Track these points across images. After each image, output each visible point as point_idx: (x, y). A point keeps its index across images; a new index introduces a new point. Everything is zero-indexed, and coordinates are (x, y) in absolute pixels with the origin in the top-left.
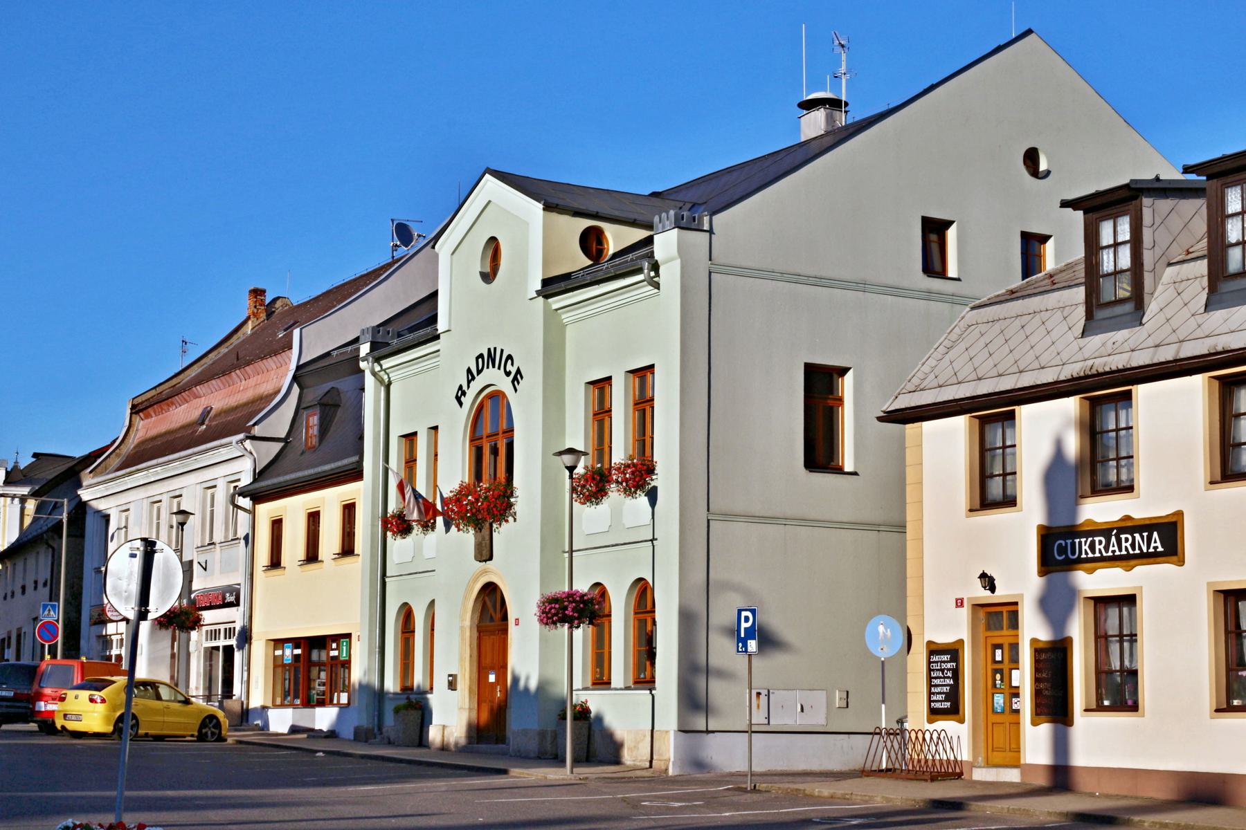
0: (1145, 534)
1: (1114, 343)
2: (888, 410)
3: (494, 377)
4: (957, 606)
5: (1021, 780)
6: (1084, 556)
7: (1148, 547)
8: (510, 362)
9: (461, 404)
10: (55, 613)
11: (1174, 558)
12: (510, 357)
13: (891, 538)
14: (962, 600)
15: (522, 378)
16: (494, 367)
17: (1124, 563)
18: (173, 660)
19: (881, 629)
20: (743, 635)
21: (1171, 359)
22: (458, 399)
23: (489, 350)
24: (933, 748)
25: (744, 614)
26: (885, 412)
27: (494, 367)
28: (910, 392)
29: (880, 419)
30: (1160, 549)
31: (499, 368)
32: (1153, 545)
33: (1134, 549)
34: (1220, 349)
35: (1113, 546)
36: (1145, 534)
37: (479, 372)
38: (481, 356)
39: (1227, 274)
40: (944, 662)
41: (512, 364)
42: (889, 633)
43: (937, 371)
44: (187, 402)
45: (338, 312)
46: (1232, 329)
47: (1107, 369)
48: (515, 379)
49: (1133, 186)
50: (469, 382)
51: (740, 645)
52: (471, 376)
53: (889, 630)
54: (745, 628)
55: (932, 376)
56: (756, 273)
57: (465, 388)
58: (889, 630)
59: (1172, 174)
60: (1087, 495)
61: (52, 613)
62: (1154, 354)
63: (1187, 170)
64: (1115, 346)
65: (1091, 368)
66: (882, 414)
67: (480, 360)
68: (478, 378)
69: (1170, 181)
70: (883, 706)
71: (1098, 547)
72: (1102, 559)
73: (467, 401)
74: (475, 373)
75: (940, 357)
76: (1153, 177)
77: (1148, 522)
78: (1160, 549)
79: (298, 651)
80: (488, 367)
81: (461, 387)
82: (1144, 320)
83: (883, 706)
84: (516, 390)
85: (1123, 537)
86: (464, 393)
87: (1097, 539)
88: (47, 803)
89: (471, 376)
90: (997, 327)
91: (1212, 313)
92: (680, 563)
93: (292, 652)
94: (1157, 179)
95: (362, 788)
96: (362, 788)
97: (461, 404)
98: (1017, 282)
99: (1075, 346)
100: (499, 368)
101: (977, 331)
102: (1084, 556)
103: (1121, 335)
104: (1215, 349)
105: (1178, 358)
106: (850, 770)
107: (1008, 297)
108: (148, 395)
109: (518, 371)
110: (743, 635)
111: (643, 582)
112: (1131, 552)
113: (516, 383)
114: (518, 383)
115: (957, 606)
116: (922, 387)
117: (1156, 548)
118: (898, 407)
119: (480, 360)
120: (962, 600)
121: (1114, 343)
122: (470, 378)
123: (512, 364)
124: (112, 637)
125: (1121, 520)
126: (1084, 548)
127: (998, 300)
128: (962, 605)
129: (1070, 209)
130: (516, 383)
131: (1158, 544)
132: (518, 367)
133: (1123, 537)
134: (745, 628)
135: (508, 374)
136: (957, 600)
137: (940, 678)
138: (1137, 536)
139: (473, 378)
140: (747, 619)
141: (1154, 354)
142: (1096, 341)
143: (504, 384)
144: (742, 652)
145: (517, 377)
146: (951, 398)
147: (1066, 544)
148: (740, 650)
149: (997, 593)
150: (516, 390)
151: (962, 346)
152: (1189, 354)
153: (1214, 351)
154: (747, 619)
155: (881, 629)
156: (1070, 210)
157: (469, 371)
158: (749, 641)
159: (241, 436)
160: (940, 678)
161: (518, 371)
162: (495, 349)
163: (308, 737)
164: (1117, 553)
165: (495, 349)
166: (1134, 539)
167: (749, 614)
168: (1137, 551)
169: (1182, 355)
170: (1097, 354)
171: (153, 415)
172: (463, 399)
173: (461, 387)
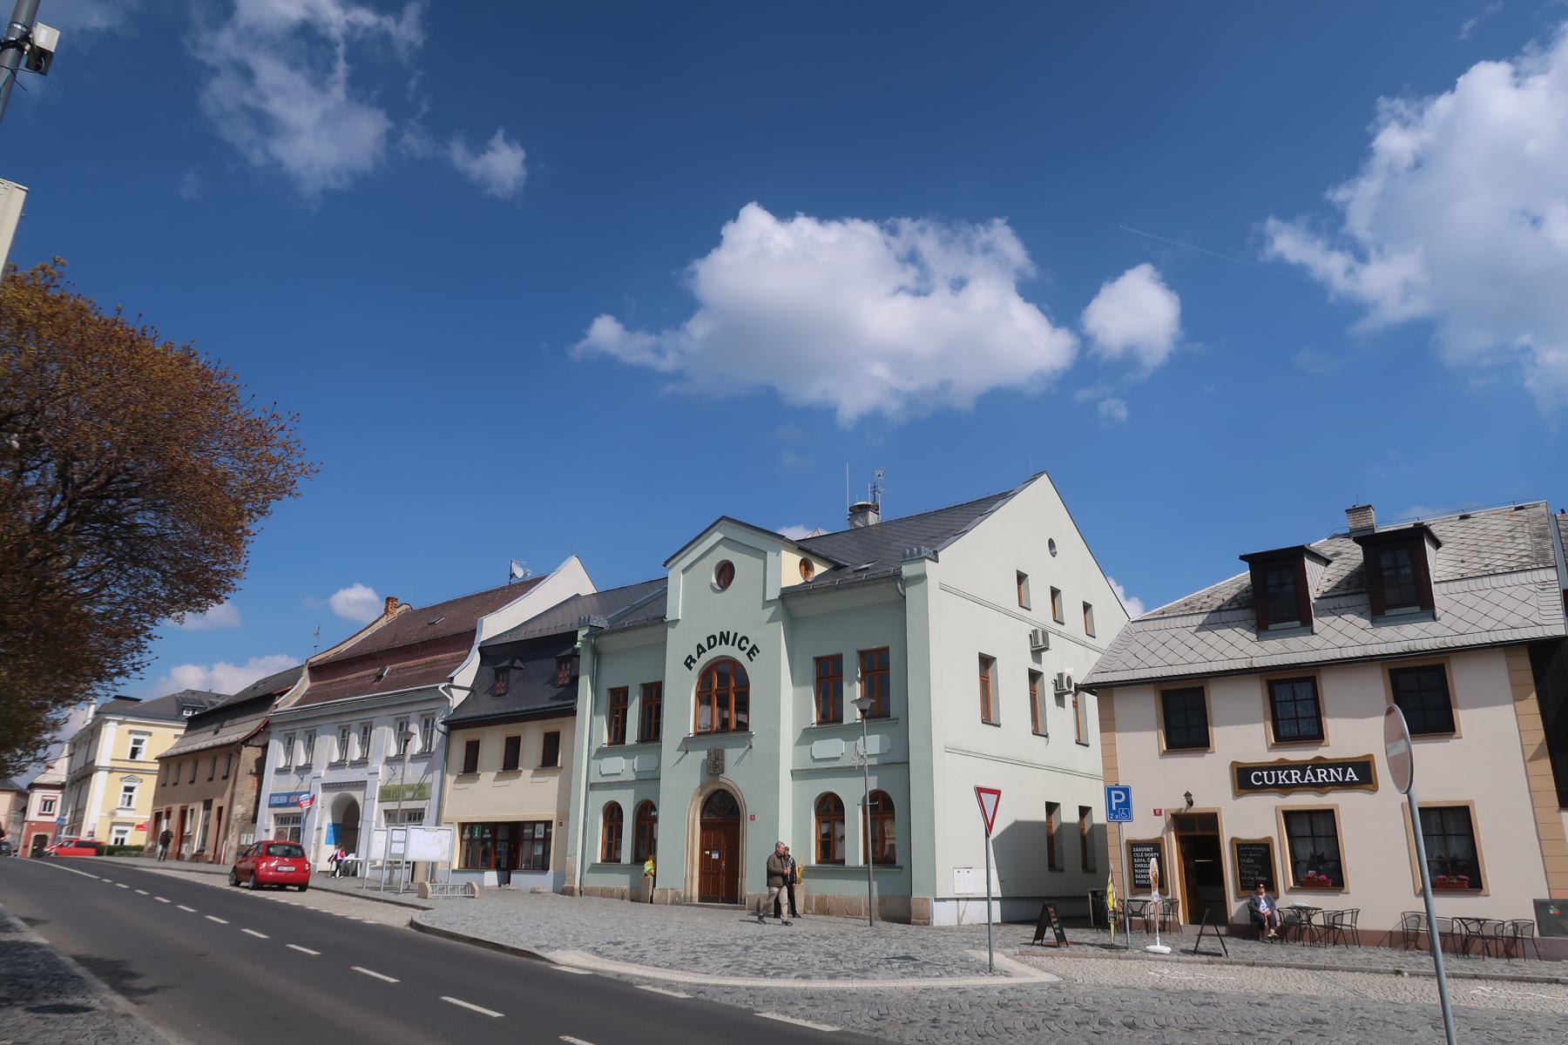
4: (1155, 814)
6: (1281, 782)
7: (1344, 777)
11: (1370, 786)
13: (907, 765)
17: (1321, 790)
25: (1113, 793)
30: (1356, 779)
31: (733, 644)
32: (1348, 776)
33: (1329, 778)
35: (1309, 776)
40: (1147, 852)
45: (699, 563)
52: (701, 650)
56: (984, 603)
70: (1326, 539)
71: (1293, 777)
72: (1298, 785)
77: (1340, 761)
78: (1356, 779)
83: (1326, 539)
85: (1319, 770)
87: (1293, 772)
88: (96, 314)
89: (700, 648)
92: (623, 782)
93: (680, 901)
97: (690, 668)
98: (128, 757)
102: (1281, 782)
111: (721, 793)
112: (1327, 780)
113: (751, 655)
115: (1089, 809)
117: (1310, 780)
126: (1280, 777)
128: (1160, 814)
130: (751, 655)
131: (1354, 775)
133: (1319, 770)
137: (1143, 863)
138: (1332, 770)
147: (1263, 774)
157: (699, 646)
160: (1143, 863)
162: (728, 633)
164: (1314, 781)
165: (728, 633)
166: (1329, 772)
168: (1332, 780)
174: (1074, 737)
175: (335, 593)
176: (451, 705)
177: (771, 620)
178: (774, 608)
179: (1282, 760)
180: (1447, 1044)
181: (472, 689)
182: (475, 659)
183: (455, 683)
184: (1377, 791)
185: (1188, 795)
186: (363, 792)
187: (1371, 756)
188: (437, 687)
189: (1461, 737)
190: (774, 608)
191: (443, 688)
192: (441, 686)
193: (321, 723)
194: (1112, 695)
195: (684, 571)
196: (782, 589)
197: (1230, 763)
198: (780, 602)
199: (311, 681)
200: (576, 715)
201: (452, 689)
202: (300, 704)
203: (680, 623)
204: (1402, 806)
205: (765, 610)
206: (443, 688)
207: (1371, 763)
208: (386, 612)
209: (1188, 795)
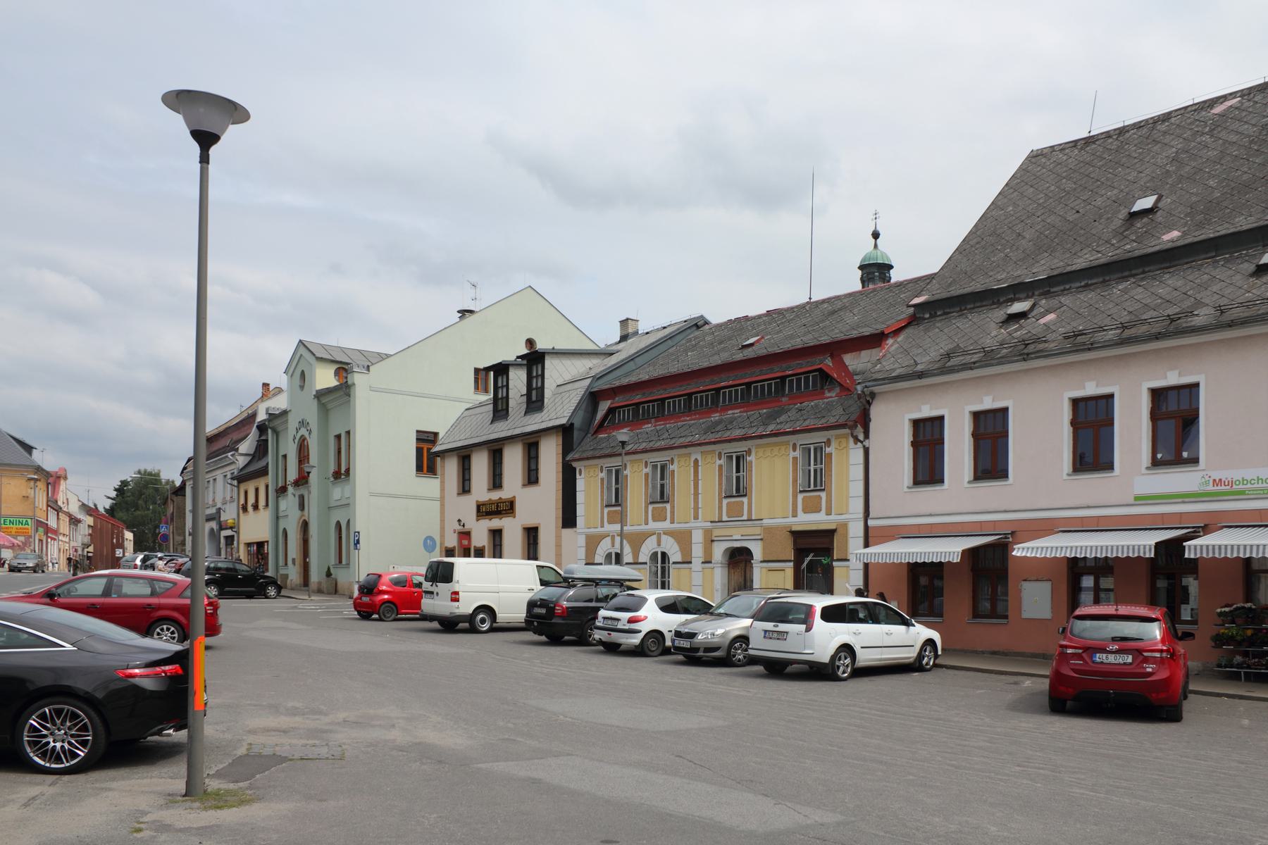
3: (303, 431)
38: (656, 553)
68: (299, 432)
76: (551, 348)
94: (553, 348)
135: (308, 430)
143: (307, 434)
159: (233, 452)
179: (490, 500)
185: (459, 521)
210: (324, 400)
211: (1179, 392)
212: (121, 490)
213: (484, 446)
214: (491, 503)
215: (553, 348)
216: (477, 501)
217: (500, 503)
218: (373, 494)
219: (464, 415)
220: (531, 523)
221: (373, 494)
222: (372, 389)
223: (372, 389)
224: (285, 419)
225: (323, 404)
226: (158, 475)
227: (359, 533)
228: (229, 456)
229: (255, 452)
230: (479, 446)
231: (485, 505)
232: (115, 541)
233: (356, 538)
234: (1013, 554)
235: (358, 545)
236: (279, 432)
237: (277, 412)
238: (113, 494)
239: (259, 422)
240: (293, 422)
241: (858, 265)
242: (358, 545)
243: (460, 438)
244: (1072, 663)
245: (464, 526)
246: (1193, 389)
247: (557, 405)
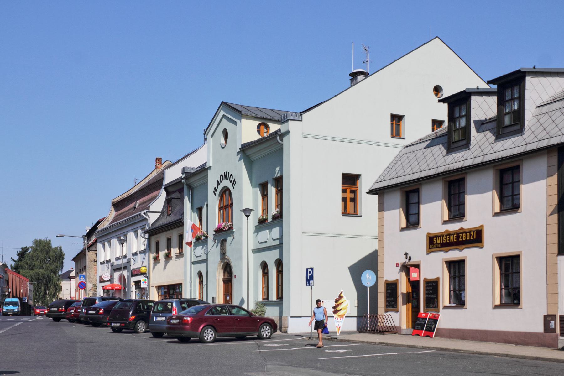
0: (460, 240)
1: (458, 157)
2: (371, 189)
3: (226, 183)
4: (397, 266)
5: (239, 305)
8: (231, 177)
9: (215, 194)
10: (84, 278)
12: (231, 175)
14: (398, 263)
15: (236, 183)
16: (226, 179)
18: (440, 349)
19: (367, 276)
20: (308, 279)
21: (480, 162)
22: (214, 192)
23: (224, 173)
24: (386, 321)
25: (309, 270)
26: (369, 190)
27: (226, 179)
28: (379, 182)
29: (368, 193)
31: (228, 180)
34: (500, 157)
36: (460, 240)
37: (221, 182)
38: (222, 175)
39: (504, 126)
41: (232, 178)
42: (370, 277)
43: (390, 173)
44: (131, 200)
46: (505, 148)
47: (455, 168)
48: (233, 183)
49: (467, 91)
50: (218, 186)
51: (307, 282)
53: (370, 276)
54: (309, 276)
55: (388, 175)
57: (216, 188)
58: (370, 276)
59: (484, 86)
60: (195, 200)
61: (83, 278)
62: (474, 160)
63: (489, 83)
64: (458, 159)
65: (449, 168)
66: (369, 191)
67: (221, 177)
68: (221, 184)
69: (483, 89)
73: (217, 193)
74: (220, 181)
75: (392, 167)
76: (475, 87)
79: (166, 290)
80: (224, 180)
81: (215, 188)
82: (471, 147)
84: (234, 188)
86: (216, 190)
90: (413, 155)
91: (497, 143)
94: (478, 88)
95: (204, 345)
96: (204, 345)
97: (215, 194)
99: (443, 160)
100: (228, 180)
101: (406, 156)
103: (463, 153)
104: (498, 157)
105: (483, 162)
106: (476, 351)
107: (419, 142)
108: (126, 196)
109: (234, 181)
110: (308, 279)
113: (233, 185)
114: (234, 185)
115: (397, 266)
116: (384, 179)
118: (374, 188)
119: (221, 177)
120: (398, 263)
121: (458, 157)
122: (218, 184)
123: (232, 178)
124: (70, 282)
125: (460, 229)
127: (415, 143)
129: (442, 103)
130: (233, 185)
132: (234, 179)
134: (309, 276)
135: (231, 182)
136: (396, 264)
139: (219, 184)
140: (310, 272)
141: (474, 160)
142: (450, 158)
143: (230, 186)
144: (308, 285)
145: (234, 183)
146: (394, 183)
148: (307, 284)
149: (411, 261)
150: (234, 188)
151: (400, 163)
152: (488, 160)
153: (498, 158)
154: (310, 272)
155: (367, 276)
156: (442, 103)
157: (218, 181)
158: (311, 281)
159: (146, 210)
161: (234, 181)
162: (226, 172)
163: (246, 337)
165: (226, 172)
167: (311, 270)
169: (485, 161)
170: (451, 162)
171: (120, 205)
172: (216, 192)
173: (215, 188)
174: (234, 239)
175: (558, 155)
176: (149, 222)
177: (240, 160)
178: (240, 155)
179: (447, 231)
180: (563, 364)
181: (162, 213)
182: (163, 195)
183: (151, 210)
184: (483, 247)
185: (406, 254)
186: (206, 263)
187: (428, 234)
188: (141, 214)
189: (521, 212)
190: (240, 155)
191: (144, 213)
192: (142, 213)
193: (110, 236)
194: (384, 196)
195: (212, 136)
196: (242, 144)
197: (199, 270)
198: (242, 153)
199: (116, 211)
200: (184, 226)
201: (148, 213)
202: (111, 224)
203: (212, 168)
204: (492, 255)
205: (238, 156)
206: (144, 213)
207: (482, 230)
208: (156, 167)
209: (406, 254)
210: (249, 152)
211: (410, 214)
212: (22, 254)
213: (397, 188)
214: (448, 234)
215: (478, 88)
216: (428, 234)
217: (462, 233)
218: (305, 234)
219: (403, 152)
220: (508, 250)
221: (305, 234)
222: (305, 136)
223: (305, 136)
224: (205, 175)
225: (248, 156)
226: (49, 243)
227: (312, 269)
228: (142, 214)
229: (163, 210)
230: (435, 177)
231: (441, 236)
232: (22, 291)
233: (309, 275)
234: (100, 312)
235: (311, 282)
236: (193, 188)
237: (192, 172)
238: (16, 258)
239: (165, 185)
240: (212, 179)
241: (437, 101)
242: (311, 282)
243: (414, 170)
244: (326, 352)
245: (410, 259)
246: (461, 206)
247: (407, 161)
